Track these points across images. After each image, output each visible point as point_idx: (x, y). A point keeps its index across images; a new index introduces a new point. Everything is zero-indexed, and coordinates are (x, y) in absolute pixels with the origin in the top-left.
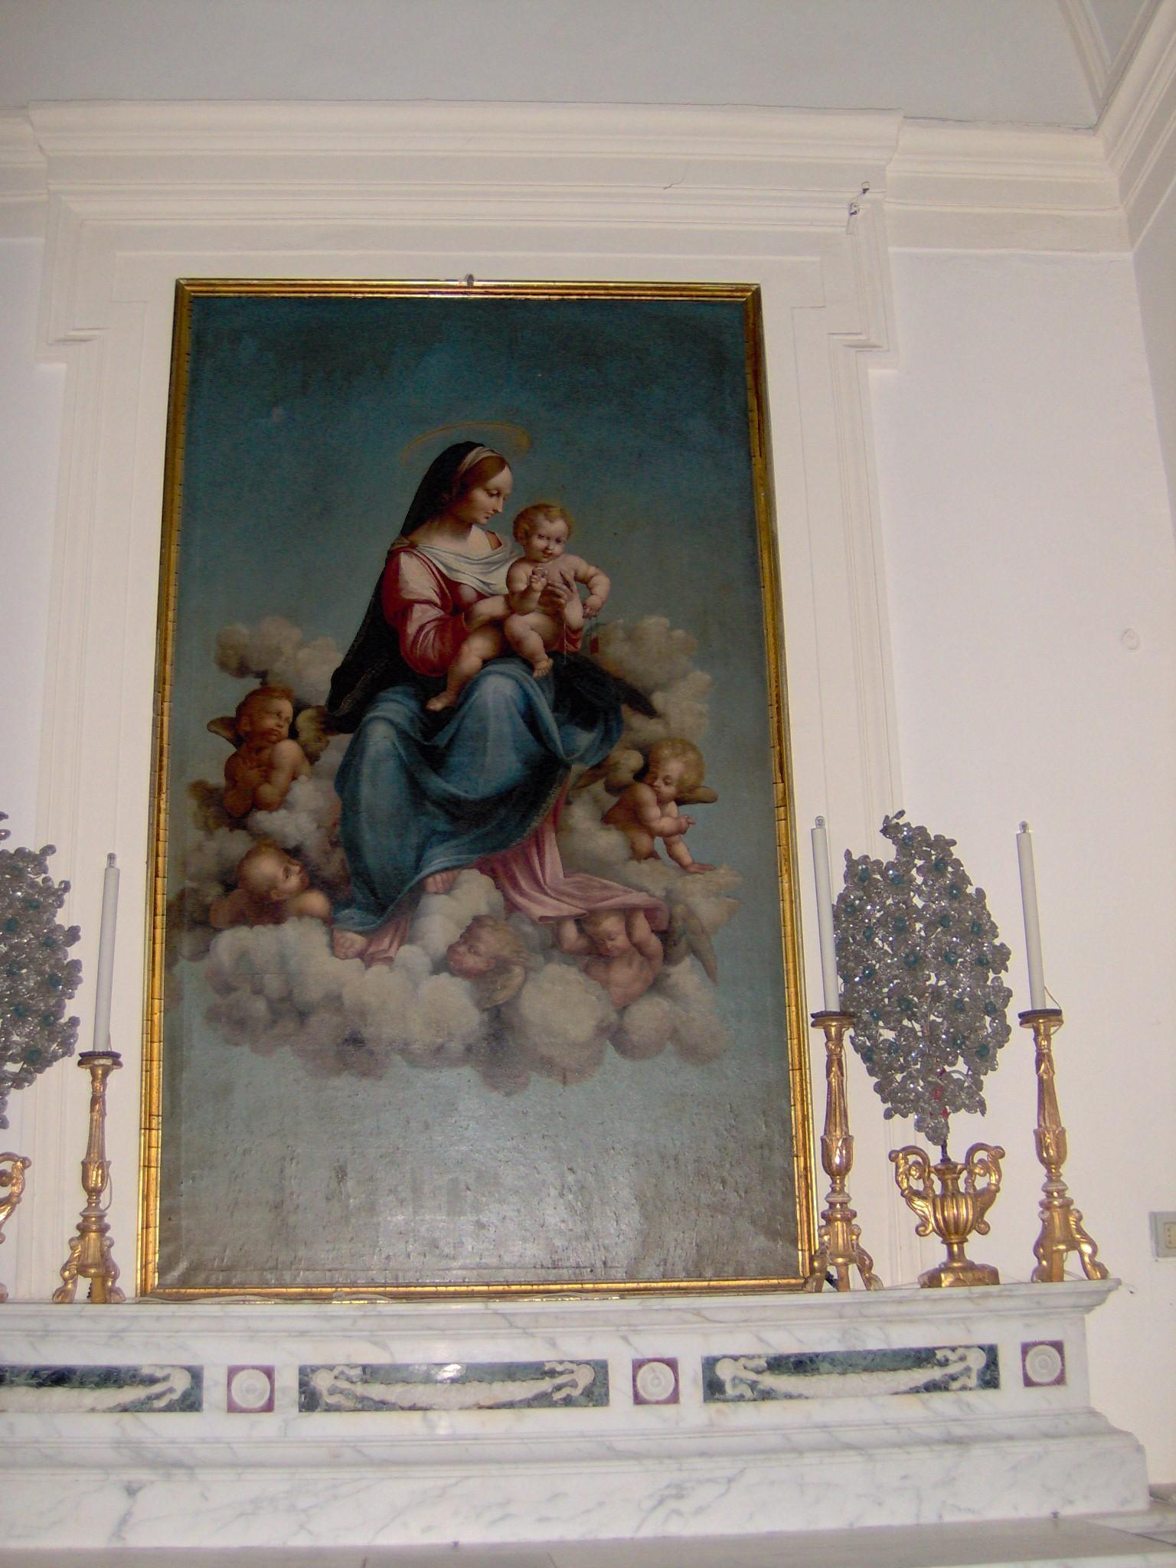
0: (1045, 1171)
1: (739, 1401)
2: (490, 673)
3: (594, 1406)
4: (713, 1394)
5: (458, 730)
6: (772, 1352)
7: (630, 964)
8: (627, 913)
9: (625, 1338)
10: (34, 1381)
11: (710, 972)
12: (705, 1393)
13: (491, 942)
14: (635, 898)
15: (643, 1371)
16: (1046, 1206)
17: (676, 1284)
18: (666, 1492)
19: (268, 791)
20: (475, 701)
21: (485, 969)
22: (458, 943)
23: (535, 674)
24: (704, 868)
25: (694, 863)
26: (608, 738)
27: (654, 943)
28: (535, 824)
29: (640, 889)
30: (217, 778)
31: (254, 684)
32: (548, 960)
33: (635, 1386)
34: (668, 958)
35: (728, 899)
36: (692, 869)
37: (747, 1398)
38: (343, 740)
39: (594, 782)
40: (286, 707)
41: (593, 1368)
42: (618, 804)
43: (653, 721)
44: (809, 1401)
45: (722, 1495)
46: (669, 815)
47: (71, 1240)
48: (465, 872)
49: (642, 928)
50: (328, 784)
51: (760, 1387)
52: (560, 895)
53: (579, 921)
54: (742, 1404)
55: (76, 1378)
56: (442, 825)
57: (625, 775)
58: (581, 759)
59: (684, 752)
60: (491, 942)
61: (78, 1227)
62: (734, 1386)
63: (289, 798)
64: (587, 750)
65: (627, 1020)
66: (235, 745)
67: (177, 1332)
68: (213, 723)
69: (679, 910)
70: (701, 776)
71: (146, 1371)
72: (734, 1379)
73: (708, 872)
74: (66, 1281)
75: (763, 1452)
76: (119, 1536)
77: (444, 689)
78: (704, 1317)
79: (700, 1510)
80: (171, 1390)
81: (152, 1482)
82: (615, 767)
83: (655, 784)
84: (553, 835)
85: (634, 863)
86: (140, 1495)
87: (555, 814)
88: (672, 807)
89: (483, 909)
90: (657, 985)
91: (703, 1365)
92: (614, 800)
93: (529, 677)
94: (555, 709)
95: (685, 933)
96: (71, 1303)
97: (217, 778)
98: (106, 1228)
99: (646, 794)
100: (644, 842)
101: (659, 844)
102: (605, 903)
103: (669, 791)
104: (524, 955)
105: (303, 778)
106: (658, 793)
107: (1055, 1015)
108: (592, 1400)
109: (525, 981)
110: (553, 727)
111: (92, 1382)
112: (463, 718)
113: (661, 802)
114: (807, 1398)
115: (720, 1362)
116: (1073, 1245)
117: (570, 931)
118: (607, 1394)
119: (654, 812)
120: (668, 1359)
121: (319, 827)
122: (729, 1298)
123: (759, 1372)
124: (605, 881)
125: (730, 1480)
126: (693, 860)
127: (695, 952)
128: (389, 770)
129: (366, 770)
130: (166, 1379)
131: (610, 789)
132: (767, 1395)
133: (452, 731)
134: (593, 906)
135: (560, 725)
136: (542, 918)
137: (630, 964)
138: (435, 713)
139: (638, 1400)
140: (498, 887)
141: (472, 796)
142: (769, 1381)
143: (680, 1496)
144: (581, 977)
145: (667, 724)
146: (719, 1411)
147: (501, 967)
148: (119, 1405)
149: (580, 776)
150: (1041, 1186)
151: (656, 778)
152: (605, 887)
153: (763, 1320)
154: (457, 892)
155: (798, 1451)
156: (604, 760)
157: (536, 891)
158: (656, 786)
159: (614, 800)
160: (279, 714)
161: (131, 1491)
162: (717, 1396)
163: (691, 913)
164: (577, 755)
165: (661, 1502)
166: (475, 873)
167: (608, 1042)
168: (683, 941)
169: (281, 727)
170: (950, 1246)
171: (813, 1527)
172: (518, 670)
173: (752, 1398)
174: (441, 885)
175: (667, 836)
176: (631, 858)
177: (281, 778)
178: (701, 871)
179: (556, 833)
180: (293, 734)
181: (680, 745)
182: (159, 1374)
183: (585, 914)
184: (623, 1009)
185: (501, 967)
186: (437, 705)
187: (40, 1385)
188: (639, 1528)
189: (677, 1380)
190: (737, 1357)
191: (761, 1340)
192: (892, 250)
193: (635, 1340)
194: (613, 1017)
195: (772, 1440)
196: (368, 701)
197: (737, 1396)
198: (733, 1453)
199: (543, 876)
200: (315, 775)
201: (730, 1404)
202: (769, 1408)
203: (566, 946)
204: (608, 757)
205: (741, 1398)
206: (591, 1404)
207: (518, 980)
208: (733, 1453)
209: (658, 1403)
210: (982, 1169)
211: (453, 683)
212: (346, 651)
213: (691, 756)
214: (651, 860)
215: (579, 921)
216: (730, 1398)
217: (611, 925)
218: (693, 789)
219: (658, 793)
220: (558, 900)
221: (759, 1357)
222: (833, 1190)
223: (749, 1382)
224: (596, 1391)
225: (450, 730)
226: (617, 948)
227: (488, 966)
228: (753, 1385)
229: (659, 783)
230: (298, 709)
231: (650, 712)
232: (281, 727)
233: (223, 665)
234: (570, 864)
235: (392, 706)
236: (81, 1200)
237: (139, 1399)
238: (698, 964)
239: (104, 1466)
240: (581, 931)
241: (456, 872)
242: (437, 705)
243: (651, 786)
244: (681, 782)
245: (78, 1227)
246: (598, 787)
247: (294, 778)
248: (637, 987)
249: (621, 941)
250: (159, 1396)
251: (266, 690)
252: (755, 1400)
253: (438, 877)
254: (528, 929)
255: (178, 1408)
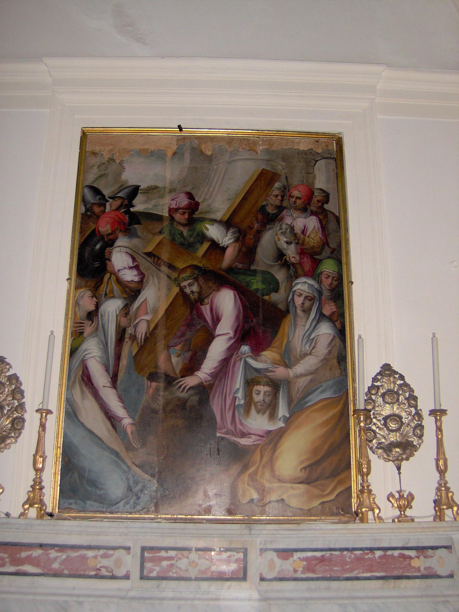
0: (439, 475)
16: (438, 489)
47: (29, 492)
61: (32, 486)
74: (25, 510)
96: (26, 518)
107: (443, 412)
116: (450, 507)
150: (437, 481)
170: (401, 512)
192: (379, 117)
222: (441, 479)
236: (32, 474)
245: (32, 486)
248: (286, 175)
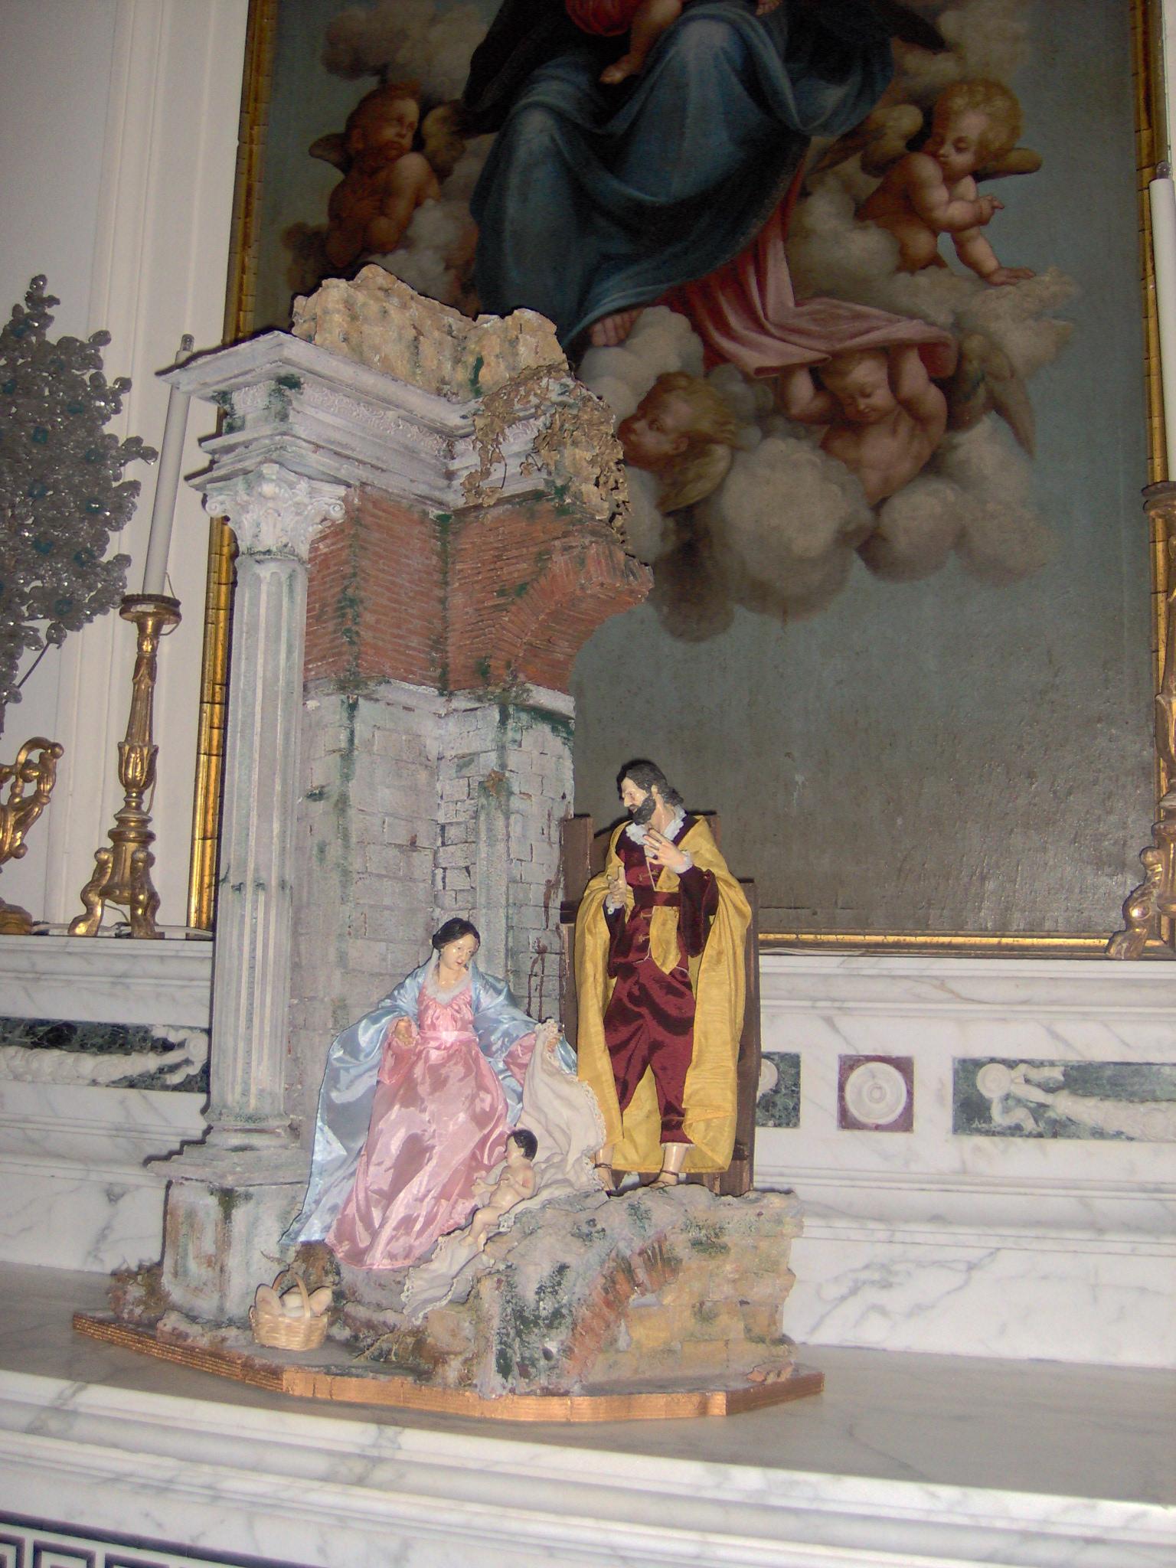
1: (1013, 1135)
2: (693, 19)
3: (775, 1126)
4: (970, 1120)
5: (641, 112)
6: (1073, 1057)
7: (894, 432)
8: (890, 354)
9: (829, 1021)
10: (28, 1040)
11: (1023, 440)
12: (956, 1117)
13: (680, 412)
14: (905, 330)
15: (856, 1077)
17: (946, 940)
18: (865, 1275)
19: (383, 227)
20: (670, 61)
21: (671, 452)
22: (634, 418)
23: (760, 12)
24: (1017, 275)
25: (1000, 268)
26: (867, 92)
27: (933, 399)
28: (754, 231)
29: (912, 316)
30: (318, 217)
31: (369, 83)
32: (767, 434)
33: (841, 1098)
34: (956, 421)
35: (1055, 322)
36: (996, 278)
37: (1026, 1132)
38: (486, 142)
39: (845, 158)
40: (410, 108)
41: (777, 1066)
42: (882, 190)
43: (940, 57)
44: (1134, 1144)
45: (960, 1288)
46: (962, 198)
48: (649, 310)
49: (914, 373)
50: (462, 208)
51: (1051, 1114)
52: (788, 332)
53: (818, 372)
54: (1018, 1141)
55: (76, 1038)
56: (619, 246)
57: (893, 143)
58: (825, 127)
59: (988, 99)
60: (680, 412)
62: (1006, 1110)
63: (410, 233)
64: (835, 114)
65: (885, 519)
66: (343, 170)
67: (192, 980)
68: (317, 145)
69: (974, 344)
70: (1014, 132)
71: (158, 1033)
72: (1007, 1097)
73: (1024, 282)
75: (1038, 1223)
76: (96, 1256)
77: (627, 52)
78: (952, 992)
79: (917, 1310)
80: (187, 1062)
81: (138, 1187)
82: (879, 133)
83: (942, 152)
84: (780, 245)
85: (903, 276)
86: (121, 1203)
87: (784, 208)
88: (967, 185)
89: (673, 364)
90: (934, 466)
91: (956, 1072)
92: (875, 183)
93: (747, 15)
94: (789, 56)
95: (983, 379)
97: (318, 217)
98: (150, 837)
99: (926, 168)
100: (921, 242)
101: (945, 243)
102: (858, 341)
103: (962, 160)
104: (731, 427)
105: (429, 203)
106: (944, 165)
108: (773, 1116)
109: (729, 469)
110: (784, 84)
111: (93, 1045)
112: (652, 89)
113: (951, 179)
114: (1131, 1139)
115: (984, 1069)
117: (802, 388)
118: (796, 1108)
119: (938, 194)
120: (898, 1058)
121: (447, 268)
122: (234, 748)
123: (1050, 1089)
124: (858, 308)
125: (971, 1267)
126: (999, 263)
127: (998, 407)
128: (545, 176)
129: (514, 180)
130: (181, 1045)
131: (871, 167)
132: (1059, 1129)
133: (637, 107)
134: (838, 346)
135: (794, 82)
136: (760, 371)
137: (894, 432)
138: (611, 86)
139: (846, 1121)
140: (697, 328)
141: (661, 200)
142: (1064, 1105)
143: (886, 1285)
144: (817, 457)
145: (961, 58)
146: (977, 1149)
147: (696, 445)
148: (125, 1077)
149: (824, 152)
151: (942, 143)
152: (858, 316)
153: (1053, 1003)
154: (635, 342)
155: (1097, 1227)
156: (861, 124)
157: (753, 331)
158: (943, 156)
159: (875, 183)
160: (400, 120)
161: (113, 1196)
162: (976, 1124)
163: (995, 346)
164: (822, 120)
165: (854, 1291)
166: (663, 310)
167: (855, 556)
168: (982, 392)
169: (402, 136)
171: (1109, 1359)
172: (734, 9)
173: (1034, 1132)
174: (612, 334)
175: (957, 230)
176: (899, 269)
177: (401, 206)
178: (1013, 280)
179: (785, 240)
180: (419, 144)
181: (981, 88)
182: (173, 1037)
183: (825, 360)
184: (878, 506)
185: (696, 445)
186: (615, 75)
187: (35, 1045)
188: (815, 1328)
189: (910, 1093)
190: (1014, 1061)
191: (1055, 1036)
193: (844, 1023)
194: (866, 516)
195: (1061, 1204)
196: (522, 81)
197: (1010, 1128)
198: (986, 1221)
199: (764, 309)
200: (444, 197)
201: (996, 1139)
202: (1061, 1149)
203: (795, 410)
204: (868, 118)
205: (1016, 1130)
206: (771, 1123)
207: (722, 465)
208: (986, 1221)
209: (878, 1128)
210: (106, 466)
211: (638, 41)
212: (492, 18)
213: (1000, 103)
214: (932, 269)
215: (818, 372)
216: (998, 1129)
217: (867, 373)
218: (1002, 153)
219: (944, 165)
220: (783, 340)
221: (1052, 1064)
223: (1032, 1105)
224: (779, 1100)
225: (633, 108)
226: (874, 409)
227: (676, 449)
228: (1038, 1110)
229: (947, 149)
230: (425, 111)
231: (934, 42)
232: (402, 136)
233: (333, 66)
234: (804, 287)
235: (555, 86)
236: (115, 798)
237: (148, 1072)
238: (1004, 425)
239: (89, 1159)
240: (819, 386)
241: (634, 313)
242: (615, 75)
243: (935, 155)
244: (983, 145)
246: (851, 166)
247: (418, 203)
248: (906, 467)
249: (881, 397)
250: (173, 1068)
251: (387, 90)
252: (1040, 1135)
253: (609, 323)
254: (738, 388)
255: (196, 1087)
